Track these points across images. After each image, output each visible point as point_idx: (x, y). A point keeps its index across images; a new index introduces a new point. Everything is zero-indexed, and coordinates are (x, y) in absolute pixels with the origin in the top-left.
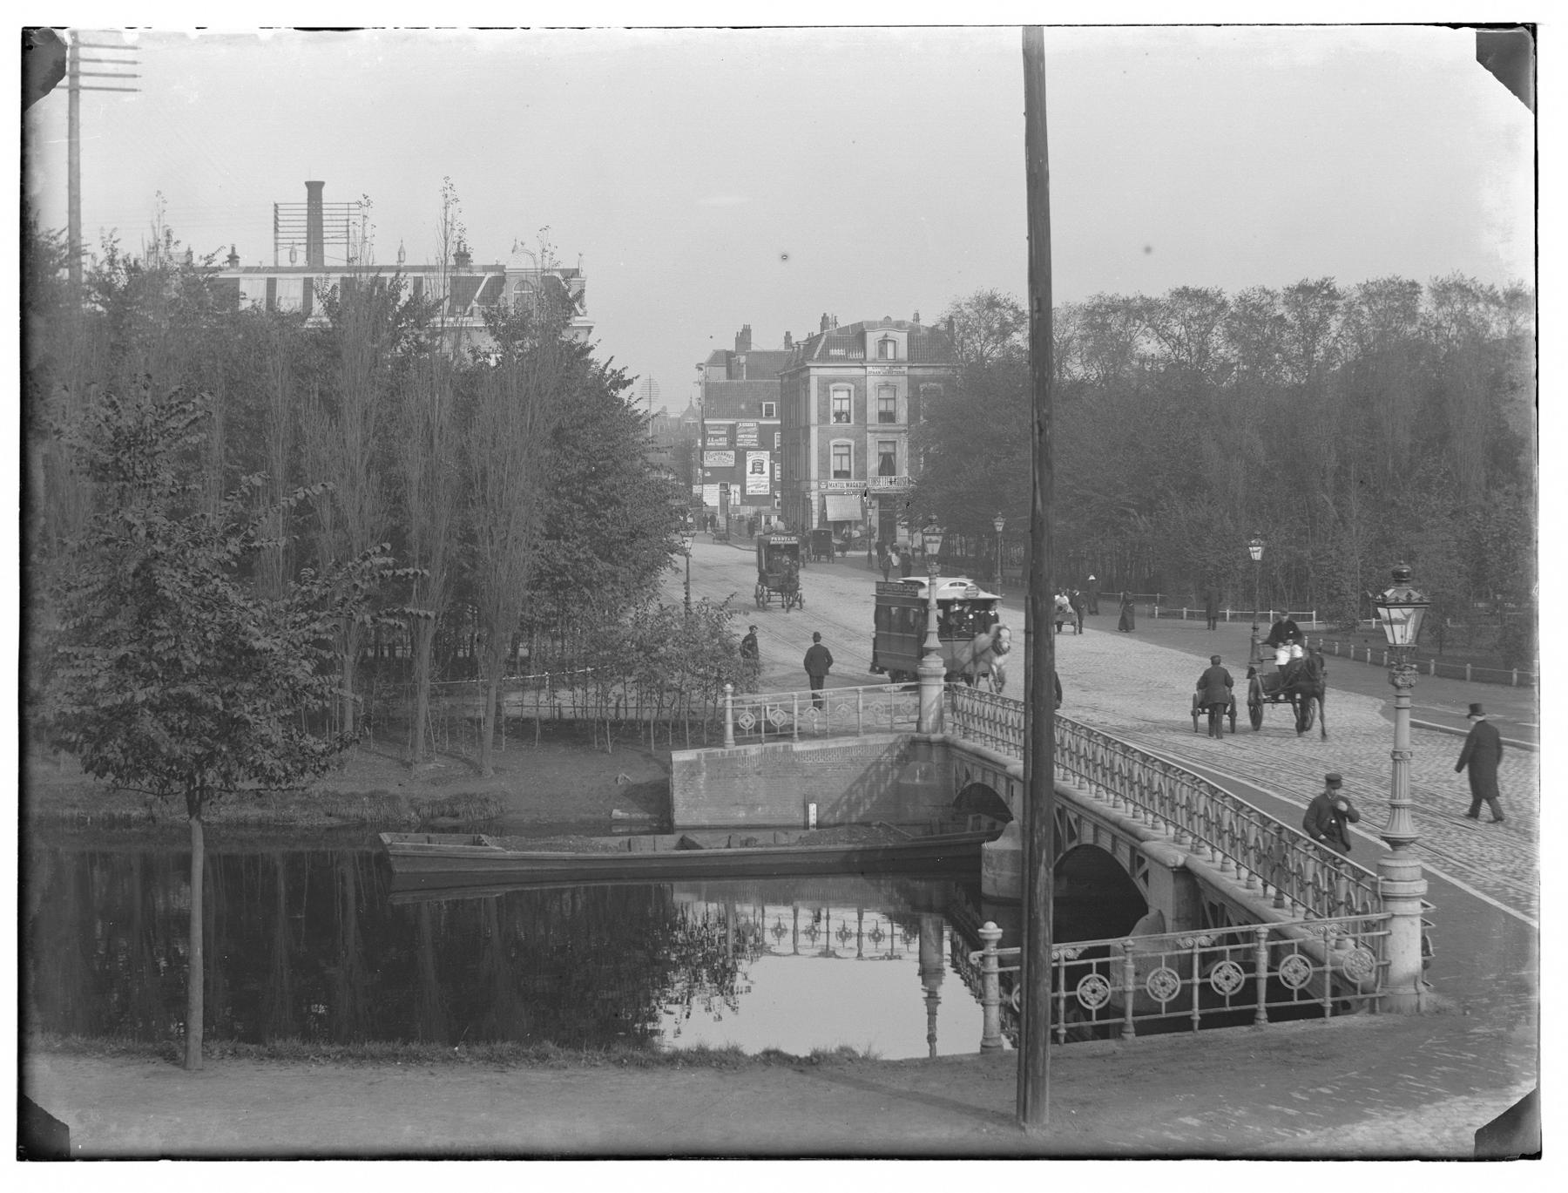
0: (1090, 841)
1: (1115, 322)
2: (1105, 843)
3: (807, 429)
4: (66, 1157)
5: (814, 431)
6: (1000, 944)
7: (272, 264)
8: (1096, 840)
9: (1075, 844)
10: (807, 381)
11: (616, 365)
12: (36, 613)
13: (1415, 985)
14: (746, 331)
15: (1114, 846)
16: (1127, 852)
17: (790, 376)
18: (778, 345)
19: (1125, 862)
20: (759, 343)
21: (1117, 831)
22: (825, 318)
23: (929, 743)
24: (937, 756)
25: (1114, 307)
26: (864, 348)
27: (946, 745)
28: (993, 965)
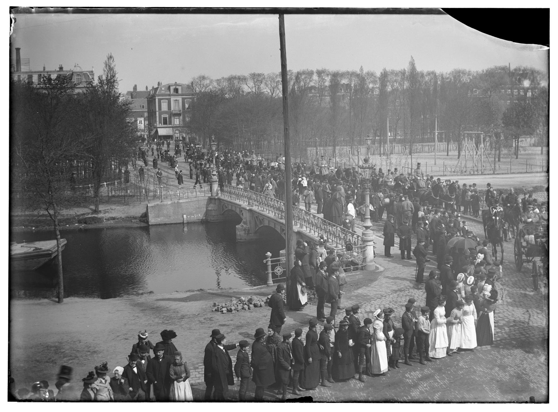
0: (267, 225)
1: (236, 82)
2: (272, 225)
3: (155, 112)
4: (175, 401)
5: (157, 113)
6: (271, 257)
7: (286, 16)
8: (269, 224)
9: (262, 225)
10: (155, 99)
11: (150, 88)
12: (15, 170)
13: (502, 259)
14: (136, 86)
15: (275, 226)
16: (279, 228)
17: (150, 98)
18: (144, 89)
19: (279, 231)
20: (139, 89)
21: (275, 222)
22: (159, 83)
23: (215, 199)
24: (217, 202)
25: (235, 78)
26: (170, 91)
27: (219, 199)
28: (269, 263)
